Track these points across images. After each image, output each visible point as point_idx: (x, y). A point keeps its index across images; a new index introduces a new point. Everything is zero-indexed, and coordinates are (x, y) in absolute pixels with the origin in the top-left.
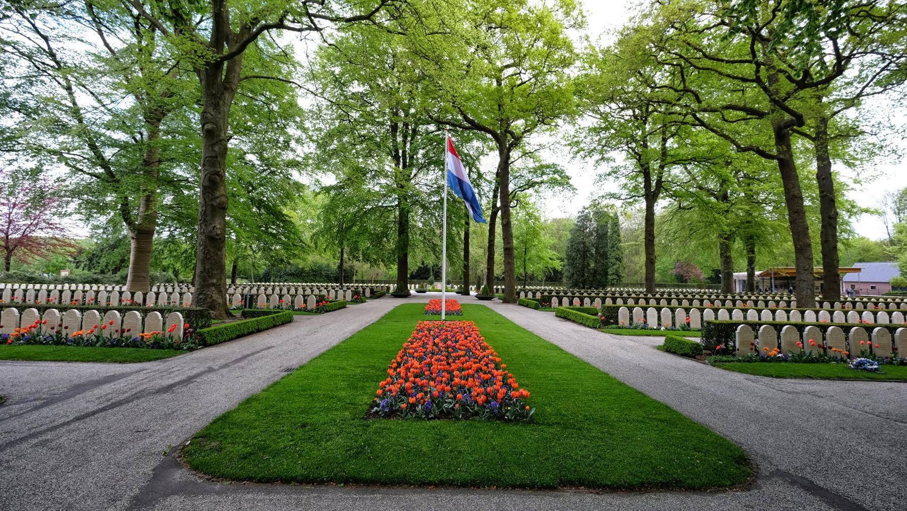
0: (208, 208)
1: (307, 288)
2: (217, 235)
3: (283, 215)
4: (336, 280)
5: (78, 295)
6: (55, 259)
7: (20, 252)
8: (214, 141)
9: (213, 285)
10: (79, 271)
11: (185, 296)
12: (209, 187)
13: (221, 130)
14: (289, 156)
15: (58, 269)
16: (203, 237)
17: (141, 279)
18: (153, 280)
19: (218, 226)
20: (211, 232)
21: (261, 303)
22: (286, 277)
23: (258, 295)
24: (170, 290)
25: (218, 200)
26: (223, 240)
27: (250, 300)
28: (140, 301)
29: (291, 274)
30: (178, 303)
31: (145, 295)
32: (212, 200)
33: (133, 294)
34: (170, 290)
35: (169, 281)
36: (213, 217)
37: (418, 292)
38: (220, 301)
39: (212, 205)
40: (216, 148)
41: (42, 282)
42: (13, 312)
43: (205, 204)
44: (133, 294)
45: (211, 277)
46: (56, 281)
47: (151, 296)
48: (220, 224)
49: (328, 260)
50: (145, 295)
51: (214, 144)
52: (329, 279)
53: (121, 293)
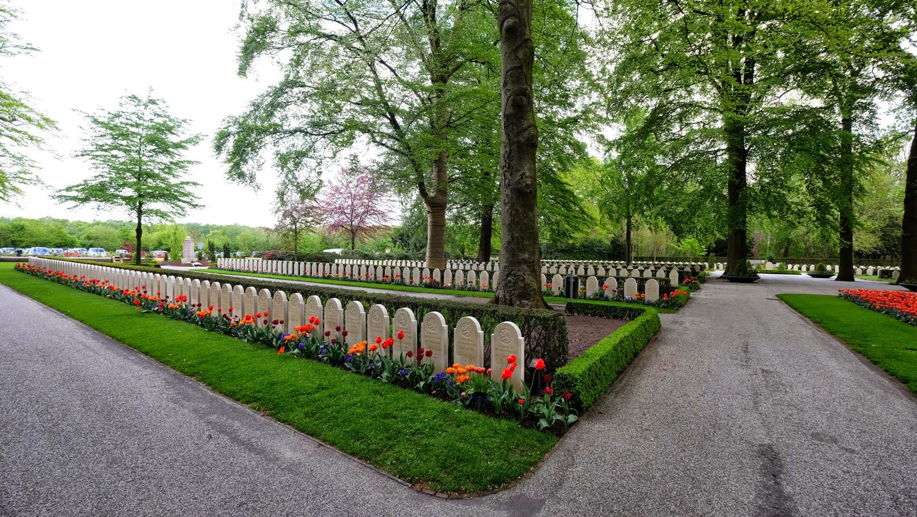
0: (514, 147)
1: (600, 267)
2: (527, 186)
3: (563, 184)
4: (611, 257)
5: (388, 272)
6: (382, 240)
7: (360, 234)
8: (518, 43)
9: (525, 261)
10: (396, 250)
11: (481, 275)
12: (513, 115)
13: (525, 26)
14: (563, 114)
15: (384, 247)
16: (508, 191)
17: (438, 257)
18: (447, 256)
19: (528, 174)
20: (518, 182)
21: (592, 287)
22: (557, 254)
23: (586, 277)
24: (602, 272)
25: (526, 134)
26: (534, 195)
27: (571, 285)
28: (438, 279)
29: (562, 251)
30: (474, 284)
31: (442, 272)
32: (518, 134)
33: (432, 271)
34: (455, 267)
35: (458, 258)
36: (521, 159)
37: (814, 276)
38: (535, 286)
39: (519, 142)
40: (521, 54)
41: (373, 258)
42: (297, 297)
43: (510, 143)
44: (432, 271)
45: (522, 250)
46: (382, 258)
47: (448, 274)
48: (530, 170)
49: (603, 232)
50: (442, 272)
51: (518, 48)
52: (602, 255)
53: (421, 269)
